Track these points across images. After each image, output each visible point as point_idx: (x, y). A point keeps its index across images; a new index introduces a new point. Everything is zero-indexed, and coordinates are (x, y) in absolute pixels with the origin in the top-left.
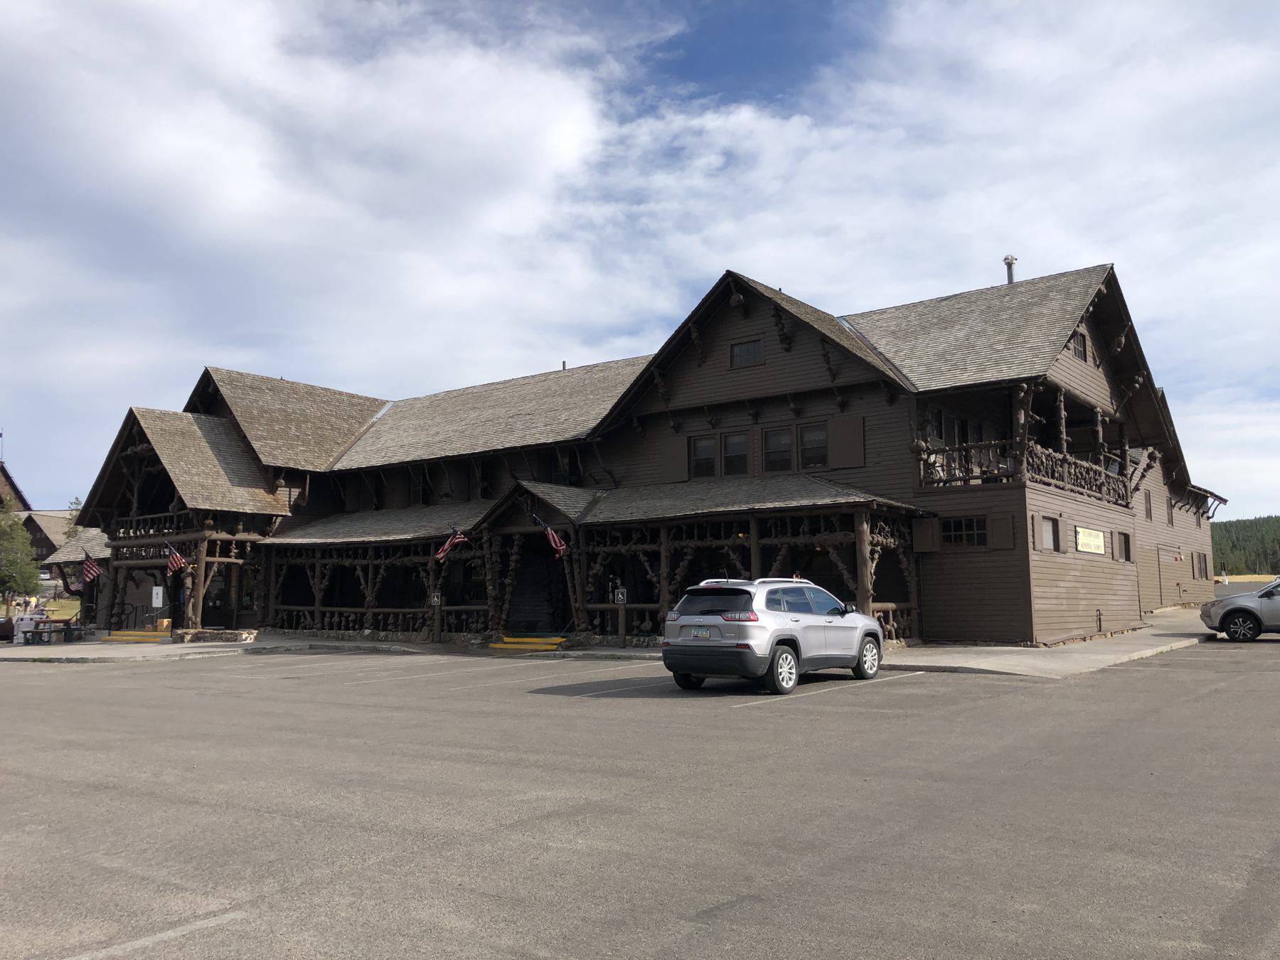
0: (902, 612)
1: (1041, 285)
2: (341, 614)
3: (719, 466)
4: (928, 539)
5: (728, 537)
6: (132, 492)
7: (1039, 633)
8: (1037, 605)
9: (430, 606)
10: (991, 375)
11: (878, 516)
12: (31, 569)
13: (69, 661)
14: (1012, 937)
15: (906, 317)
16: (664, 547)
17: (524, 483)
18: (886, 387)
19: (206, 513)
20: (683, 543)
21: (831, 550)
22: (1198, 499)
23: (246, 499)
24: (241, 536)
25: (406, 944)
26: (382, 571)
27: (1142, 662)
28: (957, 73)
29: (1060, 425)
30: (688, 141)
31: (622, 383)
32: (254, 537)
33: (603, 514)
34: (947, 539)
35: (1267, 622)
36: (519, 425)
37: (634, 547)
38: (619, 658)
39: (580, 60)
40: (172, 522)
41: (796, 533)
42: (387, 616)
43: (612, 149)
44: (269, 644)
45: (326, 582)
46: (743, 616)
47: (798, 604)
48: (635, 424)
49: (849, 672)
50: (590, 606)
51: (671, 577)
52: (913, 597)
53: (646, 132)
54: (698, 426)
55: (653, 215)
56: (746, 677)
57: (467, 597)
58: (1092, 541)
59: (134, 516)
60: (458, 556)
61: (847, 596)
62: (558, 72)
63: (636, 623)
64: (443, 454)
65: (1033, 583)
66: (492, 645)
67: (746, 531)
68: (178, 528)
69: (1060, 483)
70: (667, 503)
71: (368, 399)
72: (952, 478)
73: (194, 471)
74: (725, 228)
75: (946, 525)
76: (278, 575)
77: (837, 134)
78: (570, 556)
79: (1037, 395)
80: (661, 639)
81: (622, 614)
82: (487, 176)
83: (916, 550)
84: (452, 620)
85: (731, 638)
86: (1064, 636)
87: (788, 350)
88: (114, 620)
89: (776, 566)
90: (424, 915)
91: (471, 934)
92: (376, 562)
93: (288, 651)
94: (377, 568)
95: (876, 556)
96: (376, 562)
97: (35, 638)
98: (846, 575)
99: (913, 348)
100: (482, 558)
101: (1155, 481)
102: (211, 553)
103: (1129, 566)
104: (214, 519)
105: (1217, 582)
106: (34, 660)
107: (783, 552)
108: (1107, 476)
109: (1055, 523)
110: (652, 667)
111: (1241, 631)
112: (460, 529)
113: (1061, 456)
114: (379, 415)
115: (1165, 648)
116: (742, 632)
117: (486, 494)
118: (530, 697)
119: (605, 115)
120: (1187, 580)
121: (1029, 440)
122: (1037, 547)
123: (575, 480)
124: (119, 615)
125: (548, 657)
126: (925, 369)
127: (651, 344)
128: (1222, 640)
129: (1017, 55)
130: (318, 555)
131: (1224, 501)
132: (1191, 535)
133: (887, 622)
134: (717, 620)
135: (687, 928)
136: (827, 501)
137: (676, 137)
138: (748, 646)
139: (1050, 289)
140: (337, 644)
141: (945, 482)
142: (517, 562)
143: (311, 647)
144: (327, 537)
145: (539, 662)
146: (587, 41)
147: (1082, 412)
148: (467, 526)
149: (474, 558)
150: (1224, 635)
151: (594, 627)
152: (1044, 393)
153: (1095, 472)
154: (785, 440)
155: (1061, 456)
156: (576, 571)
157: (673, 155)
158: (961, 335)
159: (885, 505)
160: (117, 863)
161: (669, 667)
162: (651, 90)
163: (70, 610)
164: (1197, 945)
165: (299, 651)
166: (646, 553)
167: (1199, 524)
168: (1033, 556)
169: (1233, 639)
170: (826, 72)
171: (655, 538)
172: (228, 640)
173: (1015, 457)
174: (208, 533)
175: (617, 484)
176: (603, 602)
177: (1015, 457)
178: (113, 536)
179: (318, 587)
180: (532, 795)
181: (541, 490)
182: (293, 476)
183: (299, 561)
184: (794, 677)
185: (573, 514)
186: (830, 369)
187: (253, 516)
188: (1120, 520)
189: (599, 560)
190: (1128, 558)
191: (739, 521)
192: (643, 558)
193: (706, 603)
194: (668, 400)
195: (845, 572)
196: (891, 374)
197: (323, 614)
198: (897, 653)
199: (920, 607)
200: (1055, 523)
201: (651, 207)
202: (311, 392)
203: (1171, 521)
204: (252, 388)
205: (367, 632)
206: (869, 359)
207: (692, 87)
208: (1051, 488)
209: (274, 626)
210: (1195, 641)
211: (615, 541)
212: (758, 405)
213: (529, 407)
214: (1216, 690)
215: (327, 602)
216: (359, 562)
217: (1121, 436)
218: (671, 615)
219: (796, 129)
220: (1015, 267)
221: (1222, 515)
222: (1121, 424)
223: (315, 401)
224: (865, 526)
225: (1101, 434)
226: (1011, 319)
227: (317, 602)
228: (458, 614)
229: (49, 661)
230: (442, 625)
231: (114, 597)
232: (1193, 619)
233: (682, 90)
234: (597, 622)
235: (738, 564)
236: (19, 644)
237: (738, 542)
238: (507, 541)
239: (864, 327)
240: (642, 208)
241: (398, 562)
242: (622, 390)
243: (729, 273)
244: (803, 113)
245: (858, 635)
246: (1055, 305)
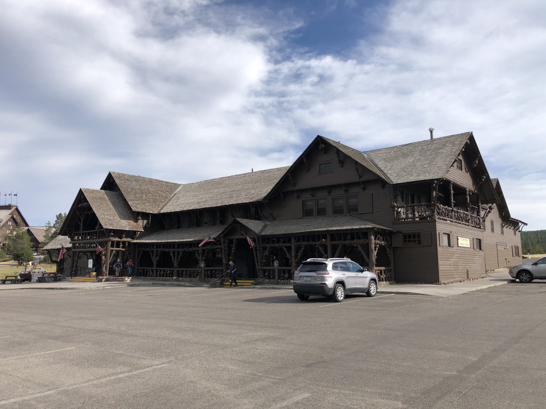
0: (387, 271)
1: (444, 140)
2: (164, 271)
3: (315, 212)
4: (398, 242)
5: (318, 241)
6: (80, 221)
7: (442, 279)
8: (441, 268)
9: (200, 268)
10: (422, 178)
11: (378, 233)
12: (30, 251)
13: (61, 289)
14: (400, 371)
15: (390, 153)
16: (293, 244)
17: (238, 219)
18: (380, 182)
20: (300, 243)
21: (359, 246)
22: (515, 224)
23: (126, 225)
24: (124, 239)
25: (219, 372)
26: (181, 253)
27: (481, 291)
28: (417, 42)
29: (451, 196)
30: (304, 71)
31: (276, 178)
33: (269, 231)
34: (405, 241)
35: (535, 274)
36: (235, 195)
37: (281, 245)
38: (276, 288)
39: (258, 39)
40: (96, 234)
41: (345, 240)
42: (182, 271)
43: (272, 75)
44: (137, 283)
45: (158, 258)
46: (323, 272)
47: (345, 268)
48: (282, 195)
49: (365, 294)
50: (264, 268)
51: (296, 256)
52: (392, 265)
53: (286, 68)
54: (306, 196)
55: (289, 102)
56: (326, 296)
57: (214, 264)
58: (464, 242)
59: (81, 231)
60: (211, 248)
61: (364, 264)
62: (250, 43)
63: (282, 275)
64: (204, 207)
65: (439, 259)
66: (225, 283)
67: (326, 238)
68: (99, 236)
69: (451, 220)
70: (294, 227)
71: (173, 184)
72: (407, 217)
73: (106, 213)
74: (320, 107)
75: (405, 236)
76: (138, 255)
77: (367, 67)
78: (256, 248)
79: (440, 186)
80: (292, 281)
81: (276, 271)
82: (218, 86)
83: (393, 246)
84: (209, 273)
85: (319, 281)
86: (453, 280)
87: (342, 167)
88: (73, 273)
89: (337, 252)
90: (222, 365)
91: (238, 370)
92: (178, 250)
93: (144, 285)
94: (178, 252)
95: (377, 249)
96: (178, 250)
97: (41, 280)
98: (365, 256)
99: (392, 165)
100: (221, 248)
101: (494, 215)
102: (112, 246)
103: (481, 252)
104: (114, 233)
105: (523, 258)
106: (47, 289)
107: (340, 247)
108: (471, 216)
109: (449, 235)
110: (289, 292)
111: (525, 278)
112: (212, 237)
113: (451, 209)
114: (178, 190)
115: (492, 285)
116: (323, 279)
117: (222, 223)
118: (243, 303)
119: (269, 61)
120: (510, 257)
122: (441, 245)
123: (257, 217)
124: (75, 271)
125: (248, 288)
126: (397, 174)
127: (288, 160)
128: (518, 282)
129: (442, 34)
130: (155, 247)
131: (526, 224)
132: (513, 239)
133: (381, 275)
134: (313, 274)
135: (302, 369)
136: (357, 227)
137: (298, 69)
138: (325, 284)
139: (447, 142)
140: (164, 282)
141: (405, 219)
142: (234, 250)
143: (153, 284)
144: (158, 240)
145: (244, 290)
146: (262, 30)
147: (460, 191)
148: (215, 236)
149: (218, 248)
150: (518, 280)
151: (266, 276)
152: (444, 185)
153: (466, 214)
154: (341, 202)
155: (451, 209)
156: (258, 254)
157: (297, 77)
158: (411, 160)
159: (380, 229)
160: (121, 352)
161: (296, 292)
162: (288, 51)
163: (52, 269)
164: (455, 373)
165: (148, 285)
166: (286, 247)
167: (515, 234)
168: (439, 249)
169: (521, 282)
170: (362, 42)
171: (289, 241)
172: (120, 281)
173: (432, 210)
174: (111, 238)
175: (274, 219)
176: (269, 266)
177: (432, 210)
178: (72, 239)
179: (155, 260)
180: (250, 334)
181: (245, 222)
182: (145, 215)
183: (147, 249)
184: (343, 296)
185: (257, 232)
186: (359, 175)
187: (129, 231)
188: (477, 233)
189: (267, 250)
190: (480, 249)
191: (324, 235)
192: (285, 249)
193: (309, 267)
194: (295, 186)
195: (365, 255)
196: (383, 177)
197: (157, 271)
198: (384, 287)
199: (395, 268)
200: (449, 235)
201: (288, 98)
202: (151, 181)
203: (502, 233)
204: (128, 180)
205: (175, 278)
206: (374, 171)
207: (306, 49)
209: (137, 275)
210: (506, 282)
211: (273, 242)
212: (330, 188)
213: (239, 187)
214: (503, 301)
215: (158, 265)
216: (172, 250)
217: (478, 200)
218: (296, 272)
219: (350, 66)
220: (434, 133)
221: (525, 229)
222: (478, 195)
223: (152, 185)
224: (372, 237)
225: (468, 199)
226: (431, 154)
227: (154, 266)
228: (211, 271)
229: (53, 289)
230: (205, 275)
231: (73, 263)
232: (504, 272)
233: (302, 50)
234: (266, 274)
235: (322, 251)
236: (34, 282)
237: (322, 243)
238: (231, 242)
239: (373, 156)
240: (284, 99)
241: (187, 250)
242: (276, 181)
243: (318, 136)
244: (352, 59)
245: (368, 280)
246: (448, 149)
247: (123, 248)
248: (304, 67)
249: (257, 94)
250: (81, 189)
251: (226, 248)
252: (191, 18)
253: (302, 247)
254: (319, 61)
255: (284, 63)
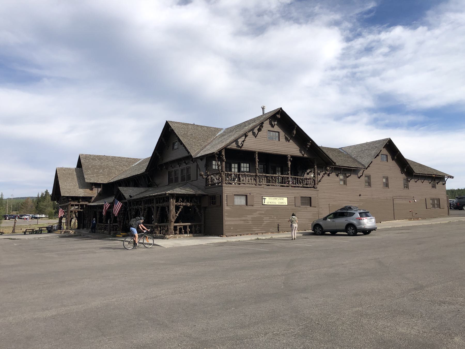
0: (195, 226)
19: (68, 197)
23: (82, 193)
30: (374, 44)
32: (87, 203)
39: (337, 23)
53: (359, 43)
55: (361, 72)
65: (225, 214)
74: (391, 73)
77: (437, 32)
82: (300, 66)
146: (337, 17)
157: (368, 50)
170: (429, 12)
182: (97, 185)
201: (361, 69)
208: (270, 187)
210: (301, 235)
248: (374, 41)
249: (333, 69)
252: (278, 15)
253: (180, 208)
254: (388, 33)
255: (356, 40)
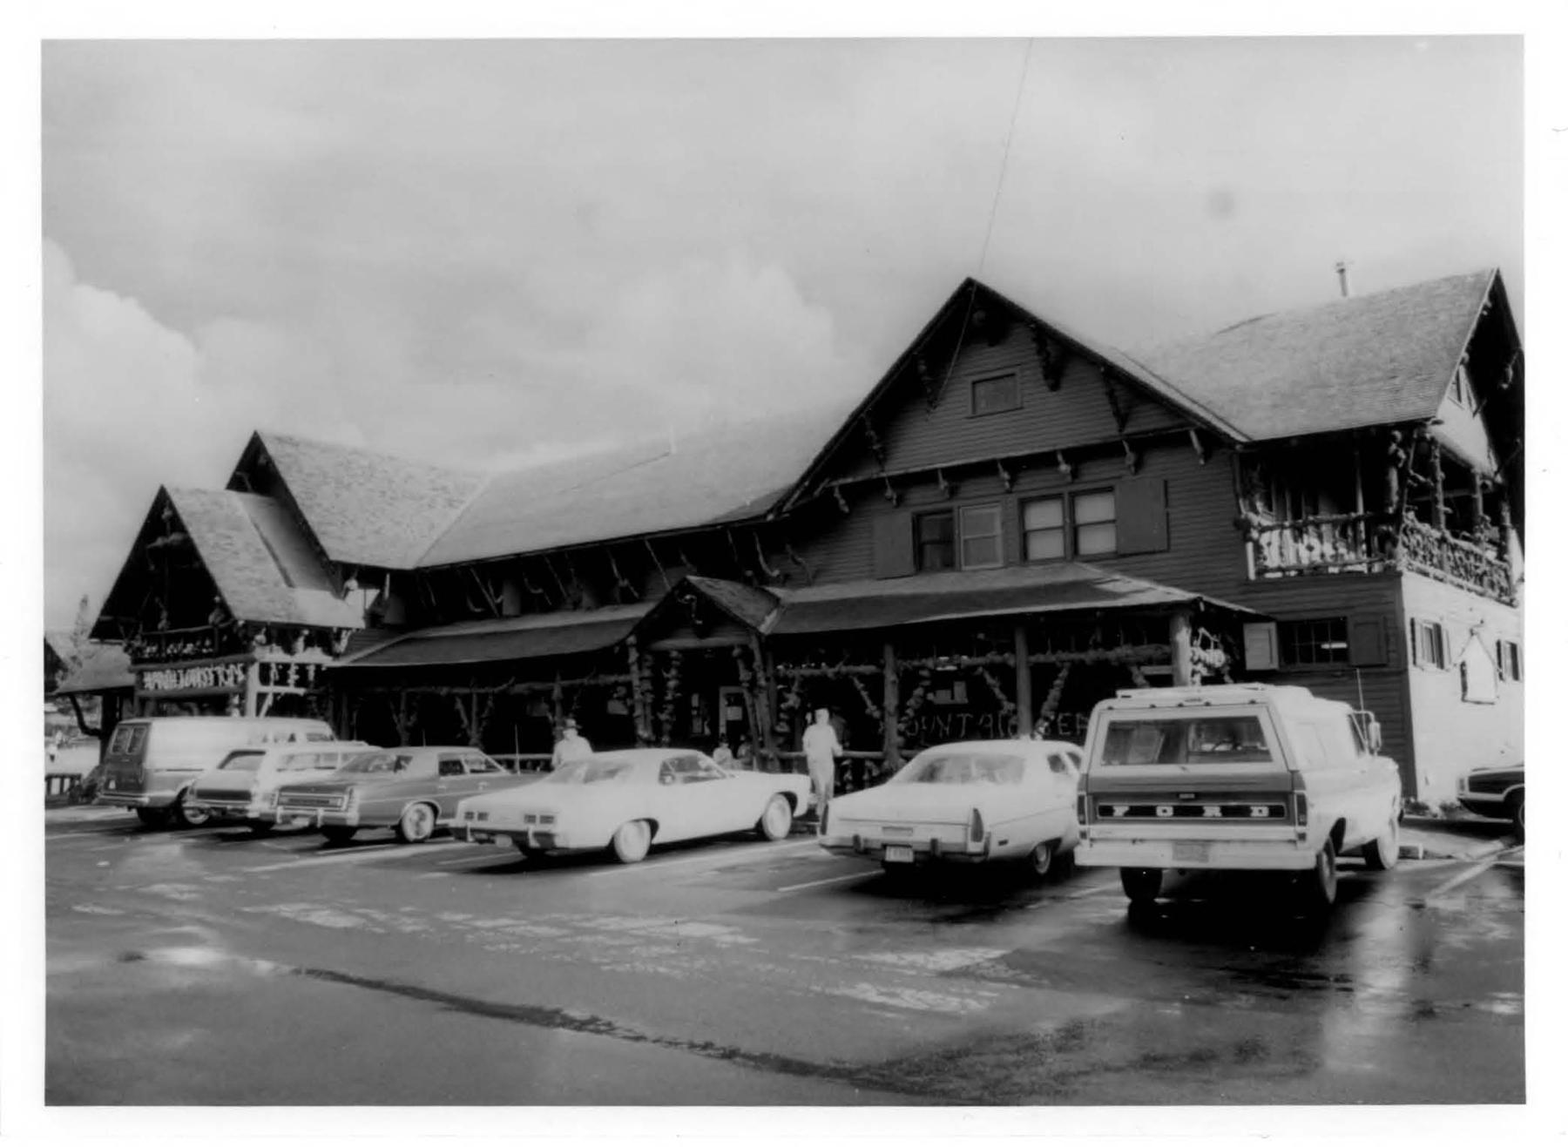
26: (490, 703)
69: (1439, 573)
100: (629, 685)
107: (1064, 673)
121: (1408, 510)
142: (676, 689)
147: (1458, 471)
155: (1436, 534)
182: (370, 576)
220: (1348, 274)
238: (663, 660)
247: (298, 684)
250: (163, 499)
251: (647, 685)
253: (1059, 670)
